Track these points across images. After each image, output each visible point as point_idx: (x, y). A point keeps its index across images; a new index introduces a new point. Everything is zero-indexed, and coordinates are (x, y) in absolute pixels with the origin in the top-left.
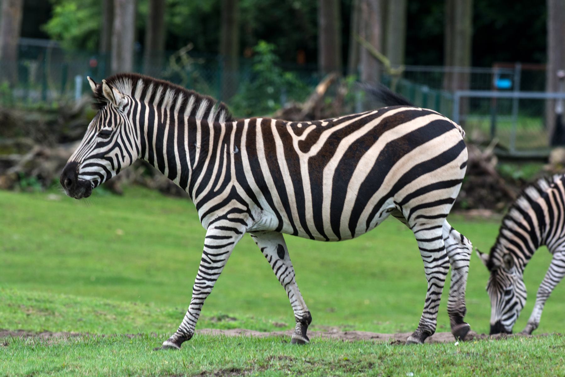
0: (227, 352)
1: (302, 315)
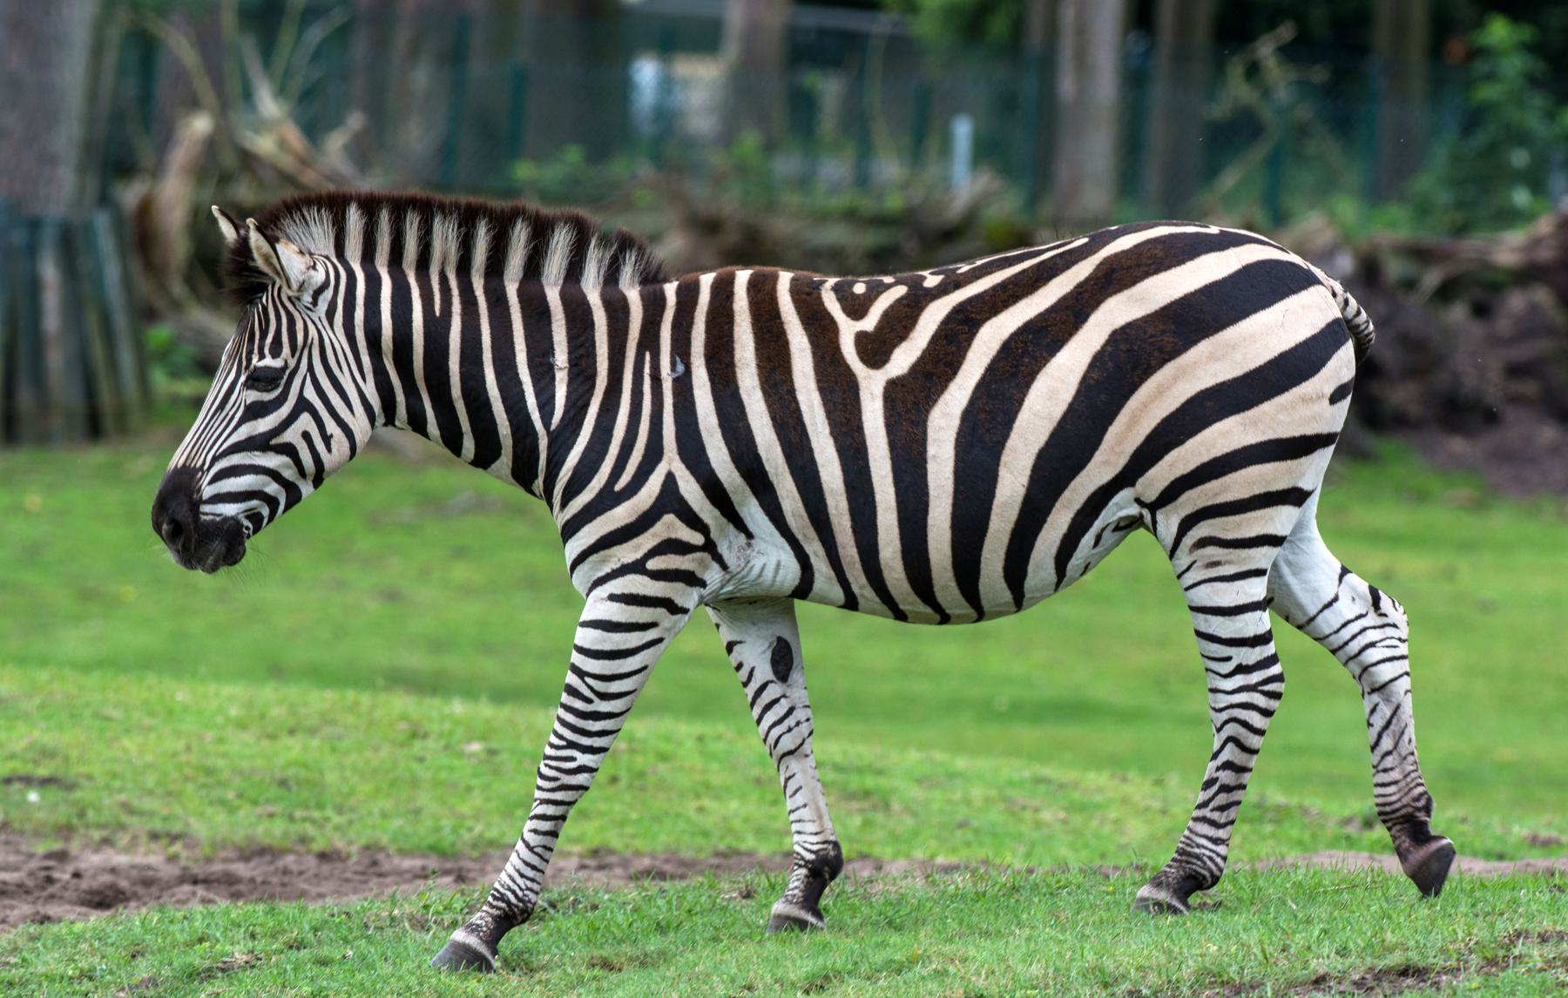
0: (1390, 918)
1: (815, 848)
